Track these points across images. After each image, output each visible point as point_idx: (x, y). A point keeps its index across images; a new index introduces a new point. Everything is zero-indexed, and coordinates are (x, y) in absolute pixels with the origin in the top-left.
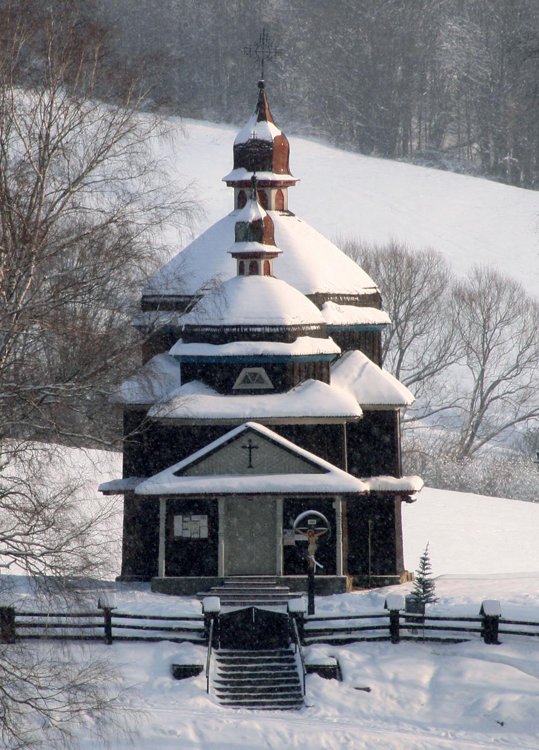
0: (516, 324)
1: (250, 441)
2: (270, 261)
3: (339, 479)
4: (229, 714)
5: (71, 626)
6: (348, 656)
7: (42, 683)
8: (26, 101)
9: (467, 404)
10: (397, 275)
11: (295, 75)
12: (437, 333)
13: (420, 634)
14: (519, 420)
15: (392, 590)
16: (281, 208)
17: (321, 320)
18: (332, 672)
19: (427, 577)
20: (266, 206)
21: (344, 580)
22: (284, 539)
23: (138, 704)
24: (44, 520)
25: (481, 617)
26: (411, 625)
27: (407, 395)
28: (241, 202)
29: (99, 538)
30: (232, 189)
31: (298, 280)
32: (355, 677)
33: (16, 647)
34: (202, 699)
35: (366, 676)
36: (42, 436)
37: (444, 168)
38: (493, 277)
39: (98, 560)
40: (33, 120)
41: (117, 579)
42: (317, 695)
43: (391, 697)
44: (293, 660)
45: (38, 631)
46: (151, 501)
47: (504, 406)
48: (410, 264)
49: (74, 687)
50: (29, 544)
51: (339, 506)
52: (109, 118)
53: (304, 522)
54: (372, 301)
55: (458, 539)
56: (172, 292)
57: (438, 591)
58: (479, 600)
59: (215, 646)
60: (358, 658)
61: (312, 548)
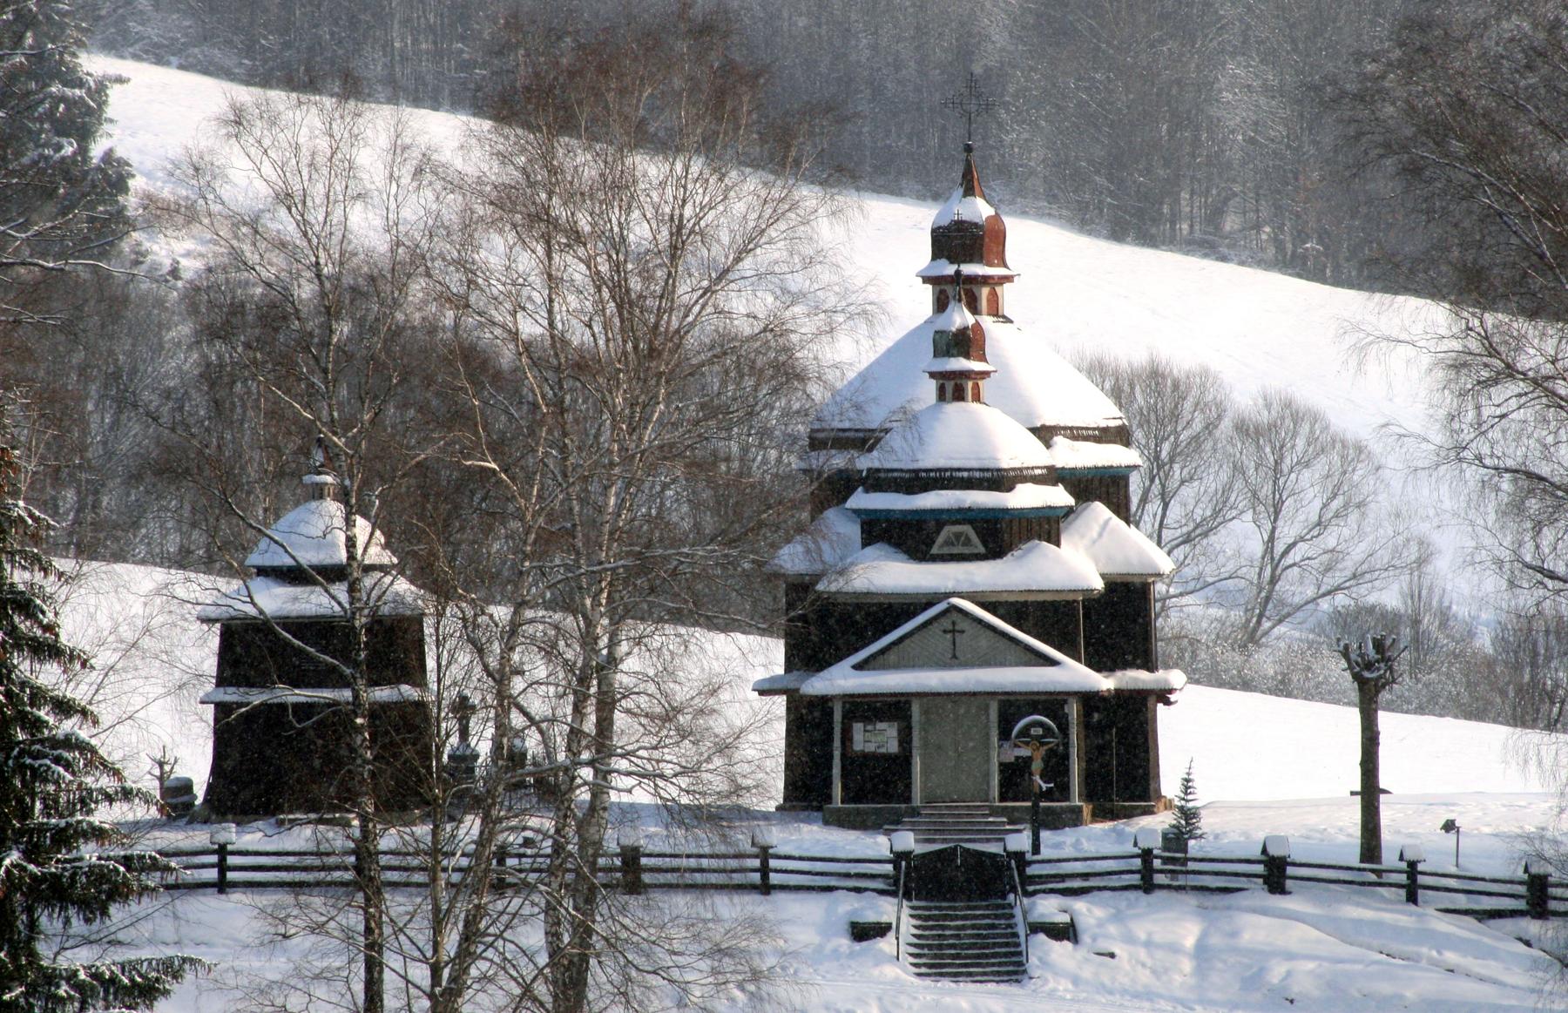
0: (1319, 466)
1: (954, 623)
2: (980, 383)
3: (1074, 674)
4: (926, 988)
5: (715, 871)
6: (1086, 911)
7: (676, 946)
8: (652, 171)
9: (1253, 574)
10: (1157, 406)
11: (1025, 136)
12: (1213, 479)
13: (1181, 881)
14: (1324, 595)
15: (1145, 821)
16: (995, 312)
17: (1048, 463)
18: (1065, 932)
19: (1190, 805)
20: (975, 310)
21: (1080, 809)
22: (1001, 754)
23: (806, 972)
24: (677, 730)
25: (1263, 858)
26: (1168, 870)
27: (1165, 564)
28: (941, 305)
29: (750, 753)
30: (929, 287)
31: (1017, 407)
32: (1094, 939)
33: (641, 898)
34: (891, 966)
35: (1107, 936)
36: (677, 617)
37: (1224, 259)
38: (1288, 404)
39: (749, 782)
40: (661, 196)
41: (778, 808)
42: (1044, 963)
43: (1144, 965)
44: (1012, 916)
45: (671, 878)
46: (823, 703)
47: (1302, 577)
48: (1176, 386)
49: (719, 951)
50: (658, 761)
51: (1073, 710)
52: (763, 193)
53: (1025, 732)
54: (1121, 436)
55: (1244, 755)
56: (847, 425)
57: (1206, 823)
58: (1260, 836)
59: (907, 896)
60: (1099, 913)
61: (1037, 766)
